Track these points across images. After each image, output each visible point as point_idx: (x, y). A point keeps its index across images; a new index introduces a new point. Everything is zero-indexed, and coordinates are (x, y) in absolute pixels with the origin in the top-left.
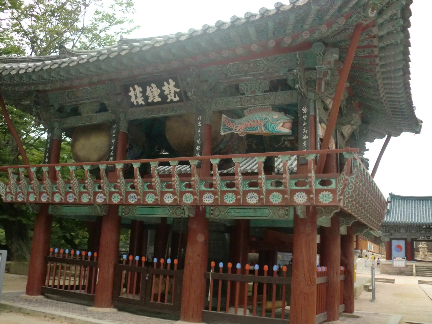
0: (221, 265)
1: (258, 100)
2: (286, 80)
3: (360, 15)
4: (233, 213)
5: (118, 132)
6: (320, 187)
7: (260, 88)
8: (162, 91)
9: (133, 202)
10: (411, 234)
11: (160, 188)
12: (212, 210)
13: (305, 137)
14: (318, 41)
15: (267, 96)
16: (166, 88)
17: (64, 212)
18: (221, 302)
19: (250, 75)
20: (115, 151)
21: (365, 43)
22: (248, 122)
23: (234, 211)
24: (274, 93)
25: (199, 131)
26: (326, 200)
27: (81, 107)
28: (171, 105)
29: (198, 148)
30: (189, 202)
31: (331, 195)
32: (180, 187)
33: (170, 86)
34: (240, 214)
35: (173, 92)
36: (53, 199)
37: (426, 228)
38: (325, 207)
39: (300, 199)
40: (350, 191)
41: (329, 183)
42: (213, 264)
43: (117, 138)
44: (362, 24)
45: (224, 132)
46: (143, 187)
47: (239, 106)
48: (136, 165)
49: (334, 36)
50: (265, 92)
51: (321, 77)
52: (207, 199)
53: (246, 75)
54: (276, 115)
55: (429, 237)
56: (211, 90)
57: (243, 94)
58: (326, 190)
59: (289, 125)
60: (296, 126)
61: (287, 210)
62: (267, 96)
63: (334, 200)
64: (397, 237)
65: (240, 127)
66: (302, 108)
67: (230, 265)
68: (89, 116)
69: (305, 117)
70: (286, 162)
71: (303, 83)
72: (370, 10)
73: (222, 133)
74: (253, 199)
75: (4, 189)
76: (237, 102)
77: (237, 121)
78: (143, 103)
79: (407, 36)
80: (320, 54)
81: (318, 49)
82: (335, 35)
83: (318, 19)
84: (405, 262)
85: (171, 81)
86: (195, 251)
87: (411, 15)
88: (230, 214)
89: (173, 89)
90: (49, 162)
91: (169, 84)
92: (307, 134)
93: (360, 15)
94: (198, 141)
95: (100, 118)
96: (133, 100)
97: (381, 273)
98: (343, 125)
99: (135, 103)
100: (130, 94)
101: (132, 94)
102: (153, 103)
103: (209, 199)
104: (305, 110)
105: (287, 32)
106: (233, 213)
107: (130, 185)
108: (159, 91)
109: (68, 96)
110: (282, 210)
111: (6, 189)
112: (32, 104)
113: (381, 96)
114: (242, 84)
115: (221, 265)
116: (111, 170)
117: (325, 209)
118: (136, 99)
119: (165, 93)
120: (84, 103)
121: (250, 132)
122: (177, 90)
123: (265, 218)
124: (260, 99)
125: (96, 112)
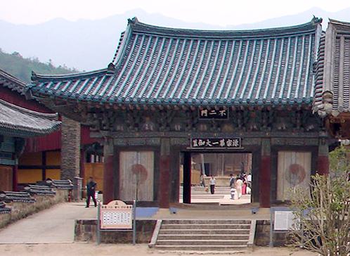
10: (171, 134)
37: (209, 116)
55: (218, 140)
64: (133, 142)
84: (134, 214)
97: (99, 244)
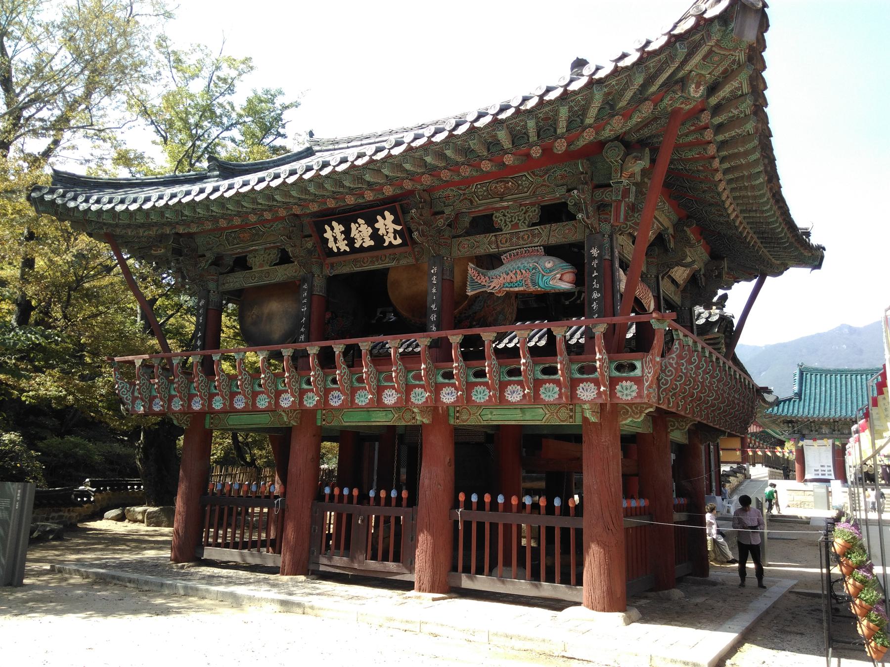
0: (474, 498)
1: (523, 238)
2: (565, 204)
3: (677, 96)
4: (490, 416)
5: (311, 295)
6: (616, 374)
7: (525, 219)
8: (376, 231)
9: (337, 404)
11: (375, 382)
12: (458, 412)
13: (595, 295)
14: (612, 141)
15: (536, 231)
16: (380, 224)
17: (231, 423)
19: (508, 201)
20: (308, 325)
21: (691, 138)
22: (508, 274)
23: (491, 413)
24: (548, 226)
25: (434, 291)
26: (627, 395)
28: (391, 251)
29: (433, 317)
30: (420, 402)
31: (635, 387)
32: (406, 379)
33: (386, 222)
34: (501, 417)
35: (391, 230)
36: (210, 405)
38: (630, 405)
39: (586, 393)
40: (669, 379)
42: (462, 497)
43: (310, 305)
44: (682, 109)
45: (473, 290)
46: (352, 381)
47: (493, 250)
48: (338, 348)
49: (638, 131)
50: (534, 225)
51: (620, 198)
52: (447, 397)
53: (502, 200)
54: (549, 263)
56: (449, 225)
59: (569, 277)
60: (580, 280)
61: (571, 410)
62: (536, 231)
63: (640, 395)
65: (498, 281)
66: (591, 249)
67: (487, 498)
68: (264, 271)
69: (595, 263)
70: (572, 332)
71: (590, 209)
72: (693, 86)
73: (470, 293)
74: (514, 395)
75: (130, 393)
76: (490, 243)
77: (492, 273)
78: (348, 249)
79: (764, 120)
80: (617, 161)
81: (613, 155)
82: (640, 129)
83: (607, 107)
85: (387, 213)
86: (435, 474)
87: (766, 88)
89: (392, 227)
90: (203, 347)
91: (384, 218)
92: (599, 291)
93: (677, 96)
94: (433, 306)
95: (282, 273)
96: (331, 244)
98: (671, 267)
99: (335, 250)
100: (325, 235)
101: (328, 235)
102: (362, 249)
103: (449, 397)
104: (595, 252)
105: (559, 131)
106: (490, 416)
107: (330, 378)
108: (370, 230)
110: (563, 410)
111: (133, 393)
112: (169, 254)
113: (732, 217)
114: (498, 215)
115: (474, 498)
116: (300, 358)
117: (631, 408)
118: (336, 243)
119: (380, 233)
120: (256, 250)
121: (511, 289)
122: (399, 228)
124: (526, 237)
125: (275, 265)
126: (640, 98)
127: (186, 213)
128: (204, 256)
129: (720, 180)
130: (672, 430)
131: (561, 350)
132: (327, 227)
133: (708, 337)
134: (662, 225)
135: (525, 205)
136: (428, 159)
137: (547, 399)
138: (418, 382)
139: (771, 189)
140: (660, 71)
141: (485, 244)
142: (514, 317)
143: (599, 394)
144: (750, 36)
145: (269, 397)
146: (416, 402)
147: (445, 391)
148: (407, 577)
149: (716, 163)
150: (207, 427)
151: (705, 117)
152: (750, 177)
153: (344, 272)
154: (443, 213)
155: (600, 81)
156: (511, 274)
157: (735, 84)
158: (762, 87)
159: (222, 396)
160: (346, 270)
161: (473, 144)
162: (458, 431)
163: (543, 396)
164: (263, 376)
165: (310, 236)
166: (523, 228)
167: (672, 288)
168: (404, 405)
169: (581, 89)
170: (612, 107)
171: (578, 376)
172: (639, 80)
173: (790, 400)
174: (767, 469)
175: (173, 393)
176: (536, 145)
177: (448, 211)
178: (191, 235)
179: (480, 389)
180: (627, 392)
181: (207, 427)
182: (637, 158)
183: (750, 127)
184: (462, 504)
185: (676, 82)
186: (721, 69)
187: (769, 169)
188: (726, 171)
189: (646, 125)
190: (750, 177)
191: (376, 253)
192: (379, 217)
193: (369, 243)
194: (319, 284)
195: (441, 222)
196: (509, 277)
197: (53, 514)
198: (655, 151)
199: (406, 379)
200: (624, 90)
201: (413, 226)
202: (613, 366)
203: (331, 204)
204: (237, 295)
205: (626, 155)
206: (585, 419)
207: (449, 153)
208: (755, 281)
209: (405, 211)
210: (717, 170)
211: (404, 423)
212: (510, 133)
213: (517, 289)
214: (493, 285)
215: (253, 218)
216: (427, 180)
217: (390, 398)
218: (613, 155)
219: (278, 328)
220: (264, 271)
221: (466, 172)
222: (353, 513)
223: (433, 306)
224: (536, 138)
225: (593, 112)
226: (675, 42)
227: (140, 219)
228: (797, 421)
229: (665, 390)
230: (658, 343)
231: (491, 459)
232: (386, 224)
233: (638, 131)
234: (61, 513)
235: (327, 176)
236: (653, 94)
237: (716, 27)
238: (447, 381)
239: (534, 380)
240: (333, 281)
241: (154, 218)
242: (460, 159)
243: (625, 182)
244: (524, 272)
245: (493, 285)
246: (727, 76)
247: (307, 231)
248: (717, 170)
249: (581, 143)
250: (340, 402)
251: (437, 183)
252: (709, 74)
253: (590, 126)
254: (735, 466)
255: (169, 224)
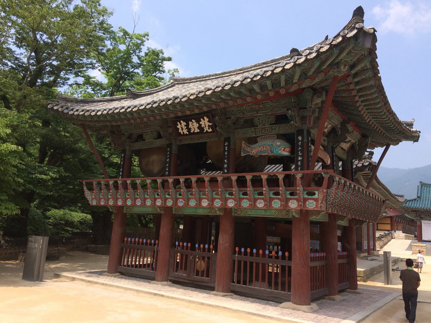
5: (171, 154)
6: (306, 196)
8: (200, 125)
9: (181, 205)
11: (198, 195)
13: (300, 158)
16: (202, 122)
18: (243, 277)
21: (344, 88)
22: (260, 147)
23: (251, 211)
27: (144, 134)
31: (315, 203)
33: (205, 122)
39: (293, 205)
41: (314, 194)
42: (237, 249)
43: (170, 158)
46: (188, 195)
49: (319, 84)
50: (272, 124)
51: (311, 114)
52: (230, 204)
54: (278, 143)
56: (234, 123)
57: (257, 126)
58: (311, 199)
59: (288, 149)
60: (293, 151)
63: (317, 206)
65: (255, 150)
67: (249, 250)
68: (150, 141)
69: (300, 143)
71: (297, 119)
73: (243, 155)
77: (253, 146)
78: (188, 133)
81: (308, 95)
85: (205, 118)
88: (248, 213)
89: (207, 124)
91: (204, 120)
92: (301, 156)
95: (159, 143)
96: (180, 131)
99: (182, 133)
100: (178, 127)
104: (300, 138)
107: (178, 193)
108: (198, 125)
109: (134, 127)
111: (92, 196)
114: (256, 119)
115: (243, 250)
122: (211, 124)
123: (272, 217)
124: (269, 130)
125: (155, 139)
126: (318, 71)
127: (116, 117)
128: (124, 134)
129: (360, 105)
130: (338, 221)
131: (281, 185)
132: (178, 123)
133: (363, 173)
134: (334, 124)
135: (269, 115)
136: (223, 96)
137: (275, 207)
138: (217, 197)
139: (386, 108)
140: (327, 60)
141: (250, 133)
142: (266, 163)
143: (299, 205)
144: (368, 45)
145: (151, 200)
146: (216, 206)
147: (230, 201)
148: (212, 285)
149: (357, 98)
150: (124, 212)
151: (349, 80)
152: (375, 104)
153: (186, 143)
154: (230, 118)
155: (299, 65)
156: (261, 147)
157: (363, 65)
158: (376, 66)
159: (131, 199)
160: (187, 142)
161: (243, 90)
162: (236, 218)
163: (273, 205)
164: (149, 191)
165: (171, 127)
166: (267, 126)
167: (342, 151)
168: (211, 206)
169: (290, 68)
170: (306, 75)
171: (289, 197)
172: (317, 64)
173: (415, 200)
174: (404, 234)
175: (110, 197)
176: (271, 91)
177: (233, 117)
178: (119, 126)
179: (245, 201)
180: (311, 205)
181: (124, 212)
182: (319, 97)
183: (372, 83)
184: (237, 253)
185: (335, 64)
186: (356, 58)
187: (384, 100)
188: (362, 102)
189: (323, 82)
190: (375, 104)
191: (200, 135)
192: (202, 119)
193: (197, 130)
194: (174, 148)
195: (230, 122)
196: (260, 148)
197: (55, 248)
198: (327, 92)
199: (212, 195)
200: (311, 68)
201: (217, 124)
202: (305, 192)
203: (180, 114)
204: (138, 153)
205: (314, 94)
206: (293, 216)
207: (232, 94)
208: (384, 147)
209: (213, 117)
210: (358, 101)
211: (211, 214)
212: (260, 85)
213: (264, 154)
214: (253, 152)
215: (145, 120)
216: (222, 105)
217: (205, 203)
218: (308, 95)
219: (156, 169)
220: (150, 141)
221: (240, 102)
222: (187, 254)
223: (226, 161)
224: (271, 88)
225: (296, 77)
226: (334, 47)
227: (96, 119)
228: (418, 211)
229: (329, 204)
230: (325, 183)
231: (251, 232)
232: (205, 122)
233: (319, 84)
234: (59, 248)
235: (178, 103)
236: (324, 69)
237: (352, 41)
238: (230, 197)
239: (269, 198)
240: (181, 148)
241: (102, 119)
242: (237, 96)
243: (313, 107)
244: (267, 146)
245: (253, 152)
246: (359, 61)
247: (170, 124)
248: (358, 101)
249: (292, 90)
250: (183, 204)
251: (227, 106)
252: (351, 60)
253: (296, 83)
254: (387, 232)
255: (108, 121)
